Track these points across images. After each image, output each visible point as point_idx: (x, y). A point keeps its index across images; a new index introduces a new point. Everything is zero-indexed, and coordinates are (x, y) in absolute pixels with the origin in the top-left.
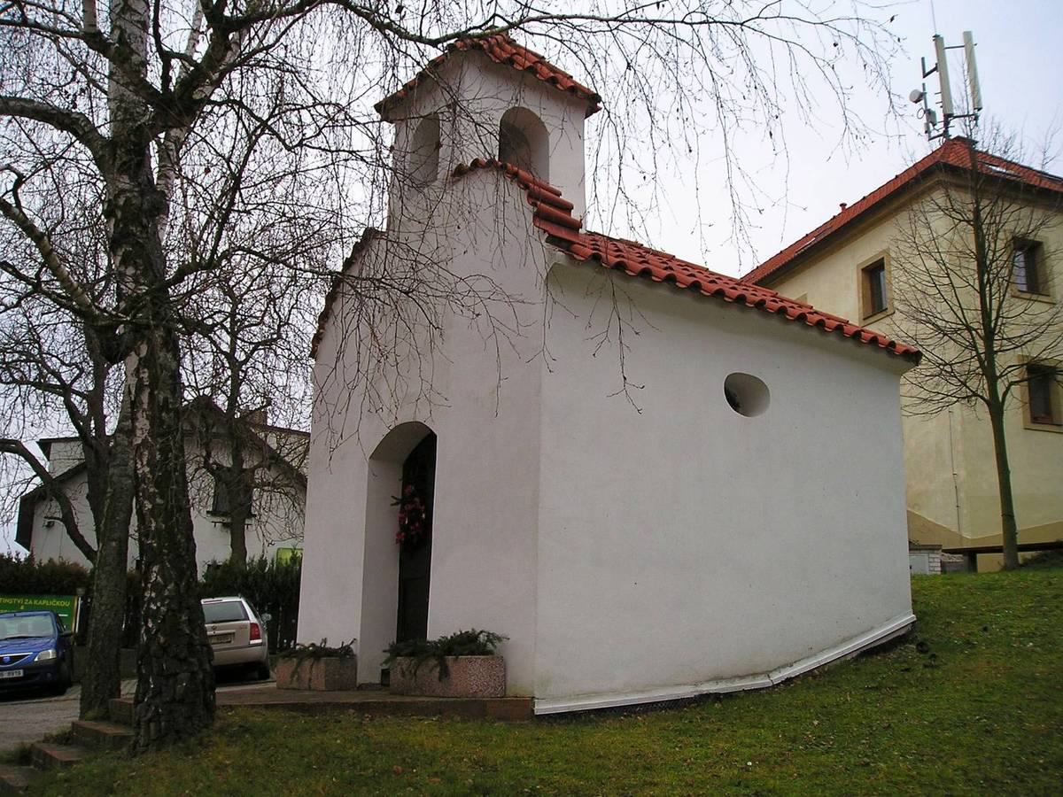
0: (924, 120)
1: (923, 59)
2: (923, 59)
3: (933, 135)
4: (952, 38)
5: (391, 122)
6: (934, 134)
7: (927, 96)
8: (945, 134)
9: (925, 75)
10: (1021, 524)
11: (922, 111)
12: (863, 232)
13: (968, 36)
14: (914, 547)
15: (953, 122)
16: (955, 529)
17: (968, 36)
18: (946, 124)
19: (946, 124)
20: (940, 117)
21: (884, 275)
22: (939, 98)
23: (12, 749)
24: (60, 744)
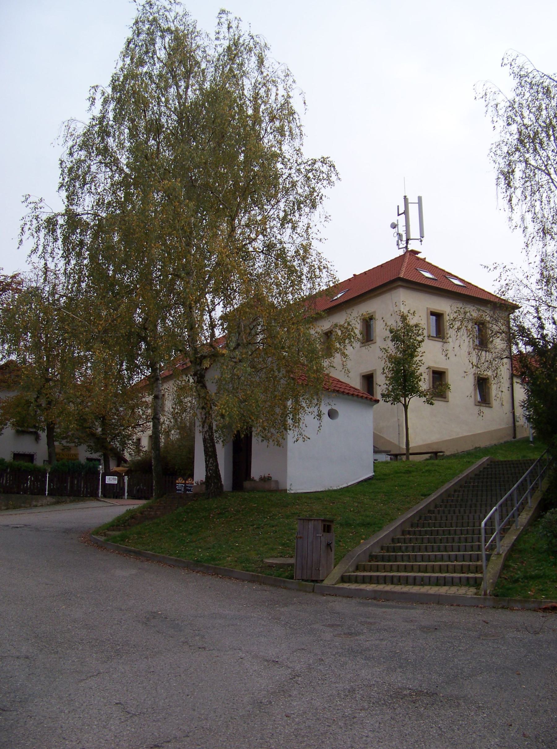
0: (396, 239)
1: (398, 206)
2: (398, 206)
3: (400, 247)
4: (413, 199)
5: (374, 472)
6: (401, 246)
7: (399, 226)
8: (406, 247)
9: (399, 215)
10: (411, 445)
11: (396, 234)
12: (364, 301)
13: (420, 198)
14: (376, 451)
15: (410, 242)
16: (397, 443)
17: (420, 198)
18: (407, 243)
19: (407, 243)
20: (404, 238)
21: (372, 322)
22: (404, 229)
23: (503, 426)
24: (100, 546)
